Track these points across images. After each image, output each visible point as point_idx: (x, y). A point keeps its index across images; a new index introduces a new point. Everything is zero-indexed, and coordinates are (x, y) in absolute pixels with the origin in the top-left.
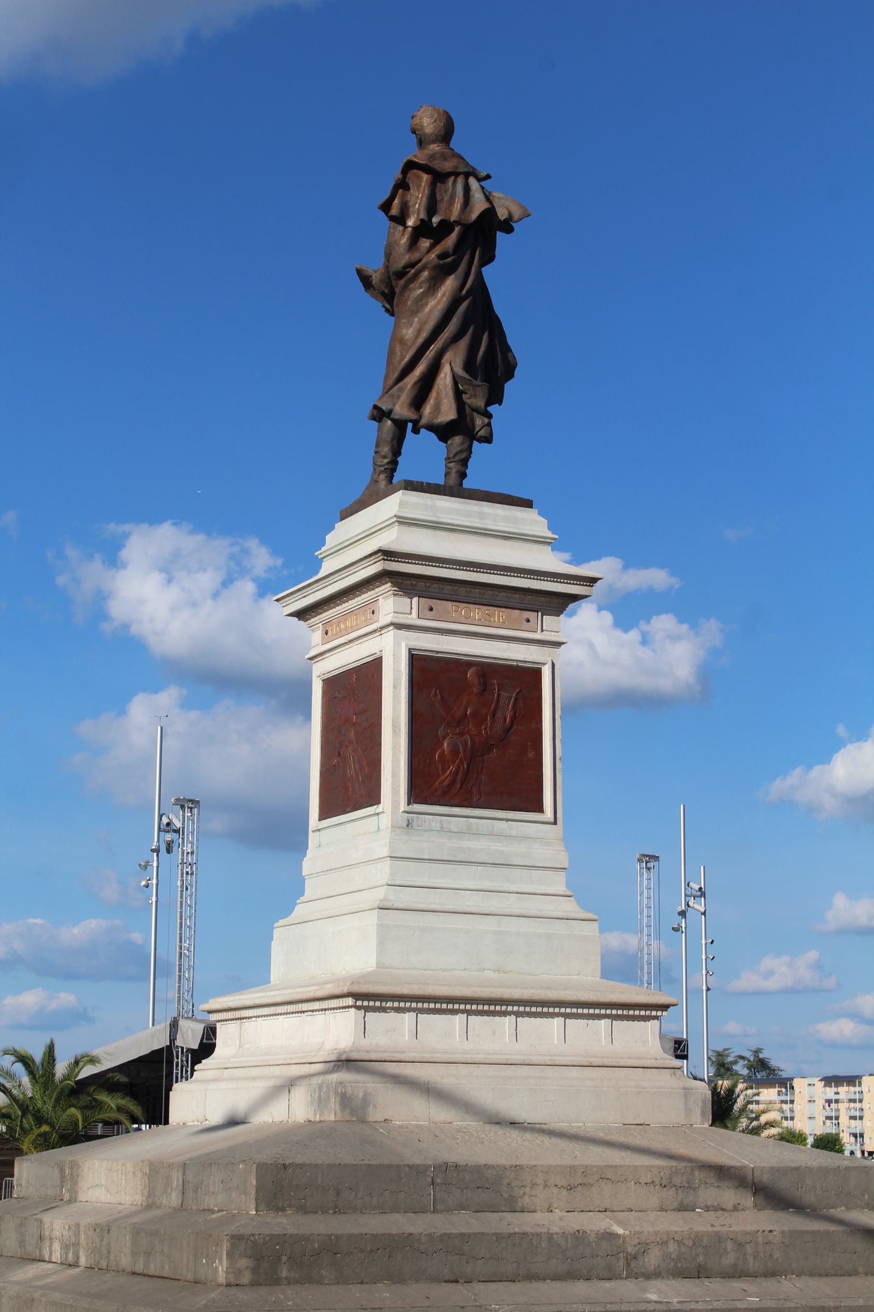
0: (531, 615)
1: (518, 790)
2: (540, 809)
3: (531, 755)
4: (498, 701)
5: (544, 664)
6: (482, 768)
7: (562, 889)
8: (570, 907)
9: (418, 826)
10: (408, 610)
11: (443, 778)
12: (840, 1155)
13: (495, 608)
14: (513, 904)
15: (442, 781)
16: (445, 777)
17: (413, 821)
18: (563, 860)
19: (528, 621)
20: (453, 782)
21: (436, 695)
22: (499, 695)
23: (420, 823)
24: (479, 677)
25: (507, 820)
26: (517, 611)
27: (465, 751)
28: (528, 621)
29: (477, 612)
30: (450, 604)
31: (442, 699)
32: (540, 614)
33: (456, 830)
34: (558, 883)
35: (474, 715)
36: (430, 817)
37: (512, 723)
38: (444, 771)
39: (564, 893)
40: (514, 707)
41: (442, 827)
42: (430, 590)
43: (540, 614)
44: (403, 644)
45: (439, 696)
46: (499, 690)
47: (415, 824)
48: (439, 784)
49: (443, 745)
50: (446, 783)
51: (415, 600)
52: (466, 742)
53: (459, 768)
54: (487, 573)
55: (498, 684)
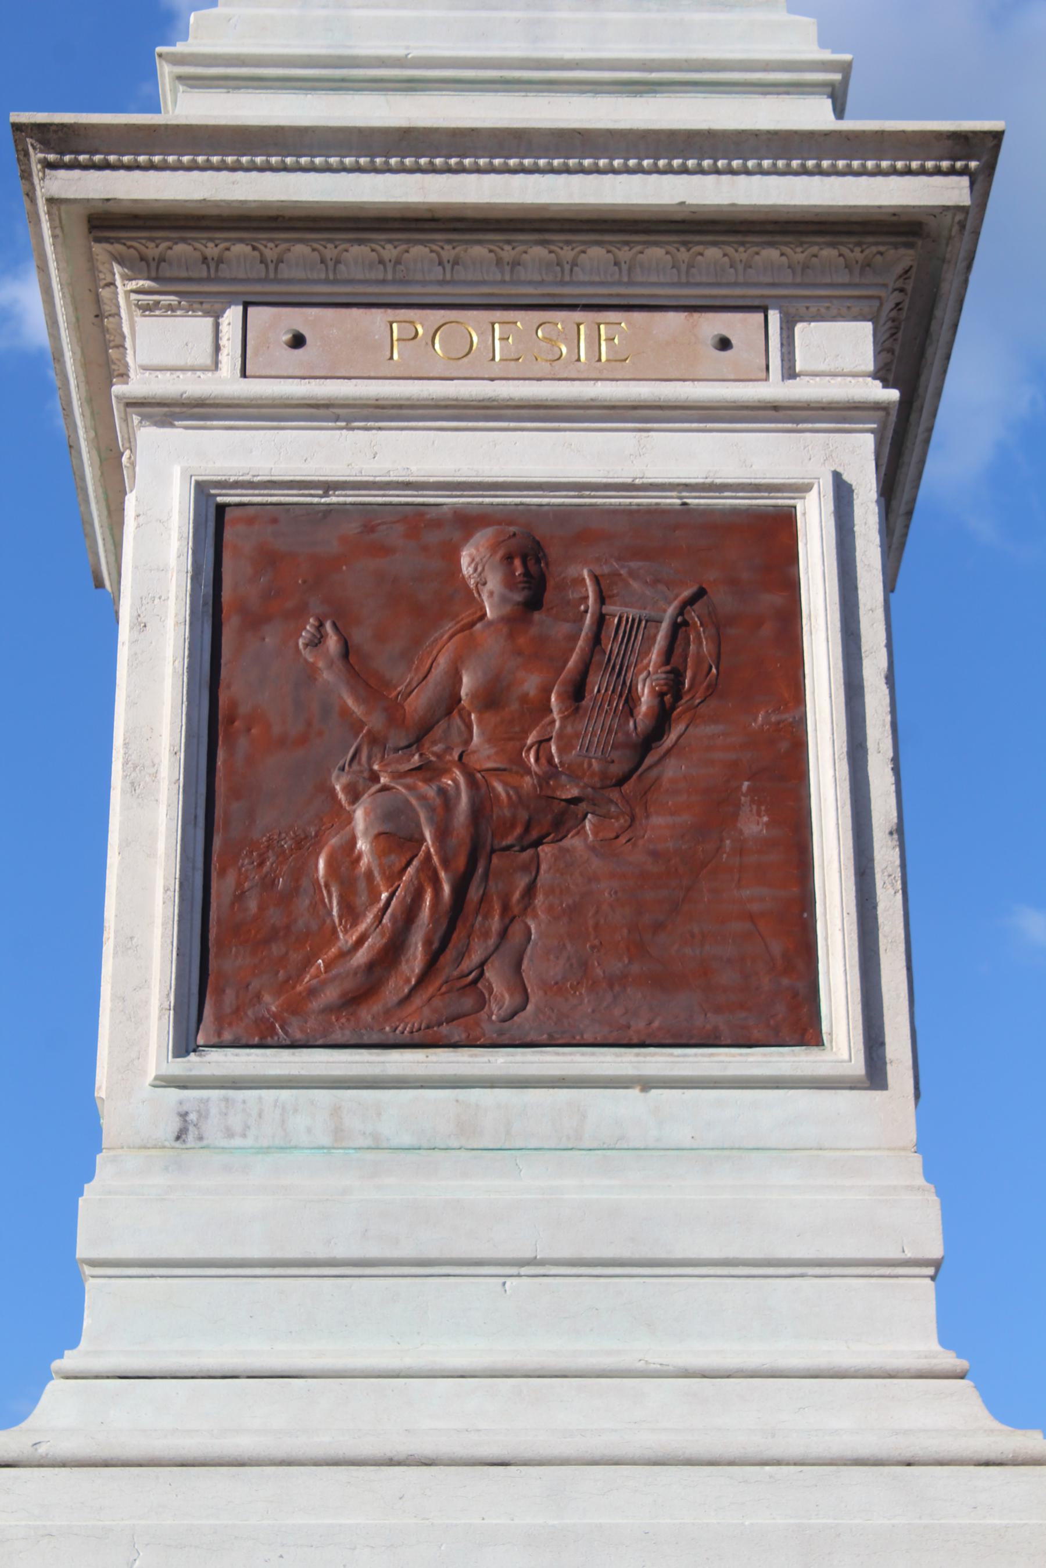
0: (740, 326)
1: (710, 960)
2: (803, 1027)
3: (753, 825)
4: (596, 639)
5: (806, 488)
6: (530, 891)
7: (924, 1346)
8: (956, 1416)
9: (230, 1134)
10: (202, 354)
11: (346, 939)
12: (854, 65)
13: (578, 316)
14: (660, 1416)
15: (345, 954)
16: (360, 940)
17: (203, 1115)
18: (919, 1224)
19: (724, 344)
20: (392, 953)
21: (317, 641)
22: (601, 620)
23: (235, 1121)
24: (509, 558)
25: (647, 1084)
26: (671, 315)
27: (442, 834)
28: (724, 344)
29: (495, 335)
30: (379, 316)
31: (346, 651)
32: (774, 316)
33: (407, 1140)
34: (906, 1322)
35: (491, 698)
36: (285, 1094)
37: (662, 719)
38: (351, 913)
39: (922, 1364)
40: (668, 654)
41: (338, 1132)
42: (285, 272)
43: (774, 316)
44: (177, 471)
45: (332, 642)
46: (602, 599)
47: (212, 1129)
48: (328, 966)
49: (350, 819)
50: (361, 956)
51: (233, 315)
52: (447, 800)
53: (418, 896)
54: (492, 170)
55: (596, 579)
